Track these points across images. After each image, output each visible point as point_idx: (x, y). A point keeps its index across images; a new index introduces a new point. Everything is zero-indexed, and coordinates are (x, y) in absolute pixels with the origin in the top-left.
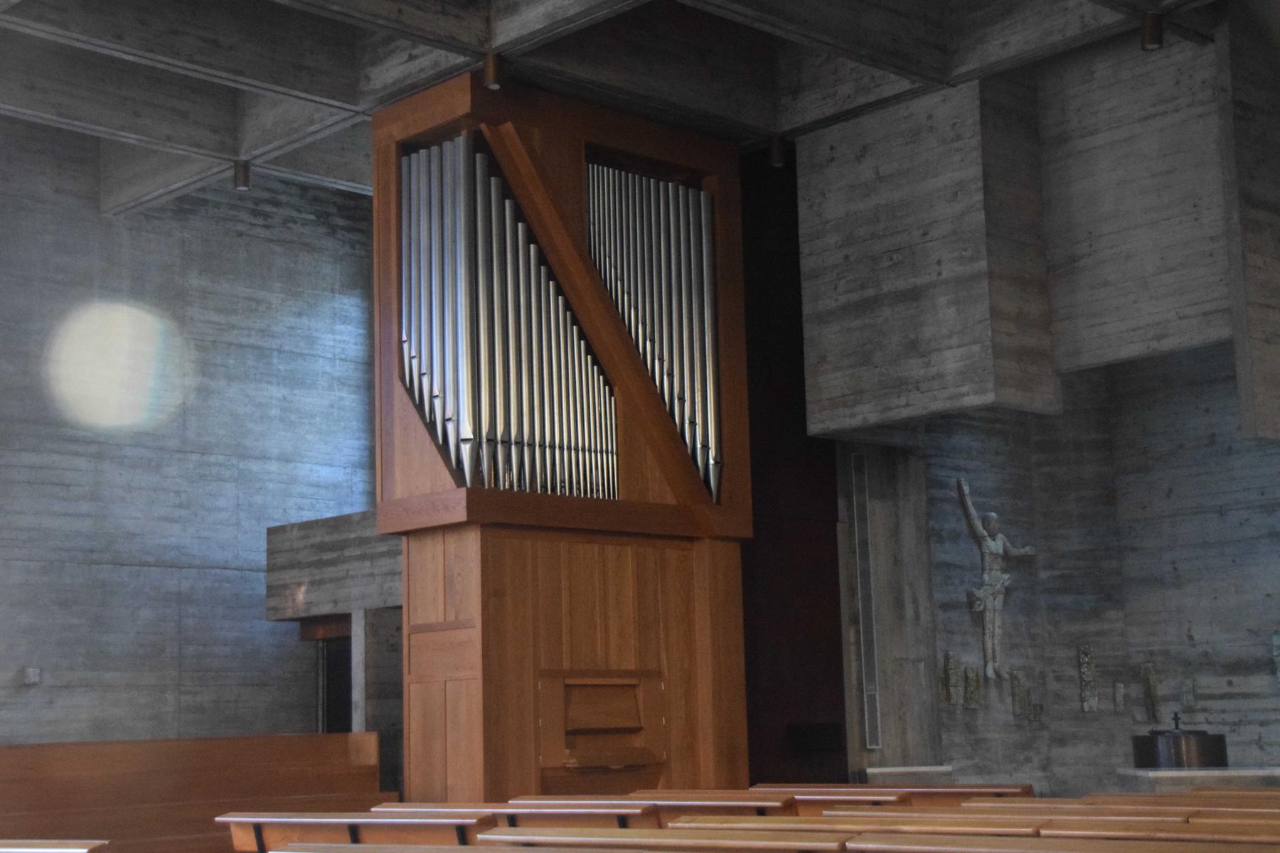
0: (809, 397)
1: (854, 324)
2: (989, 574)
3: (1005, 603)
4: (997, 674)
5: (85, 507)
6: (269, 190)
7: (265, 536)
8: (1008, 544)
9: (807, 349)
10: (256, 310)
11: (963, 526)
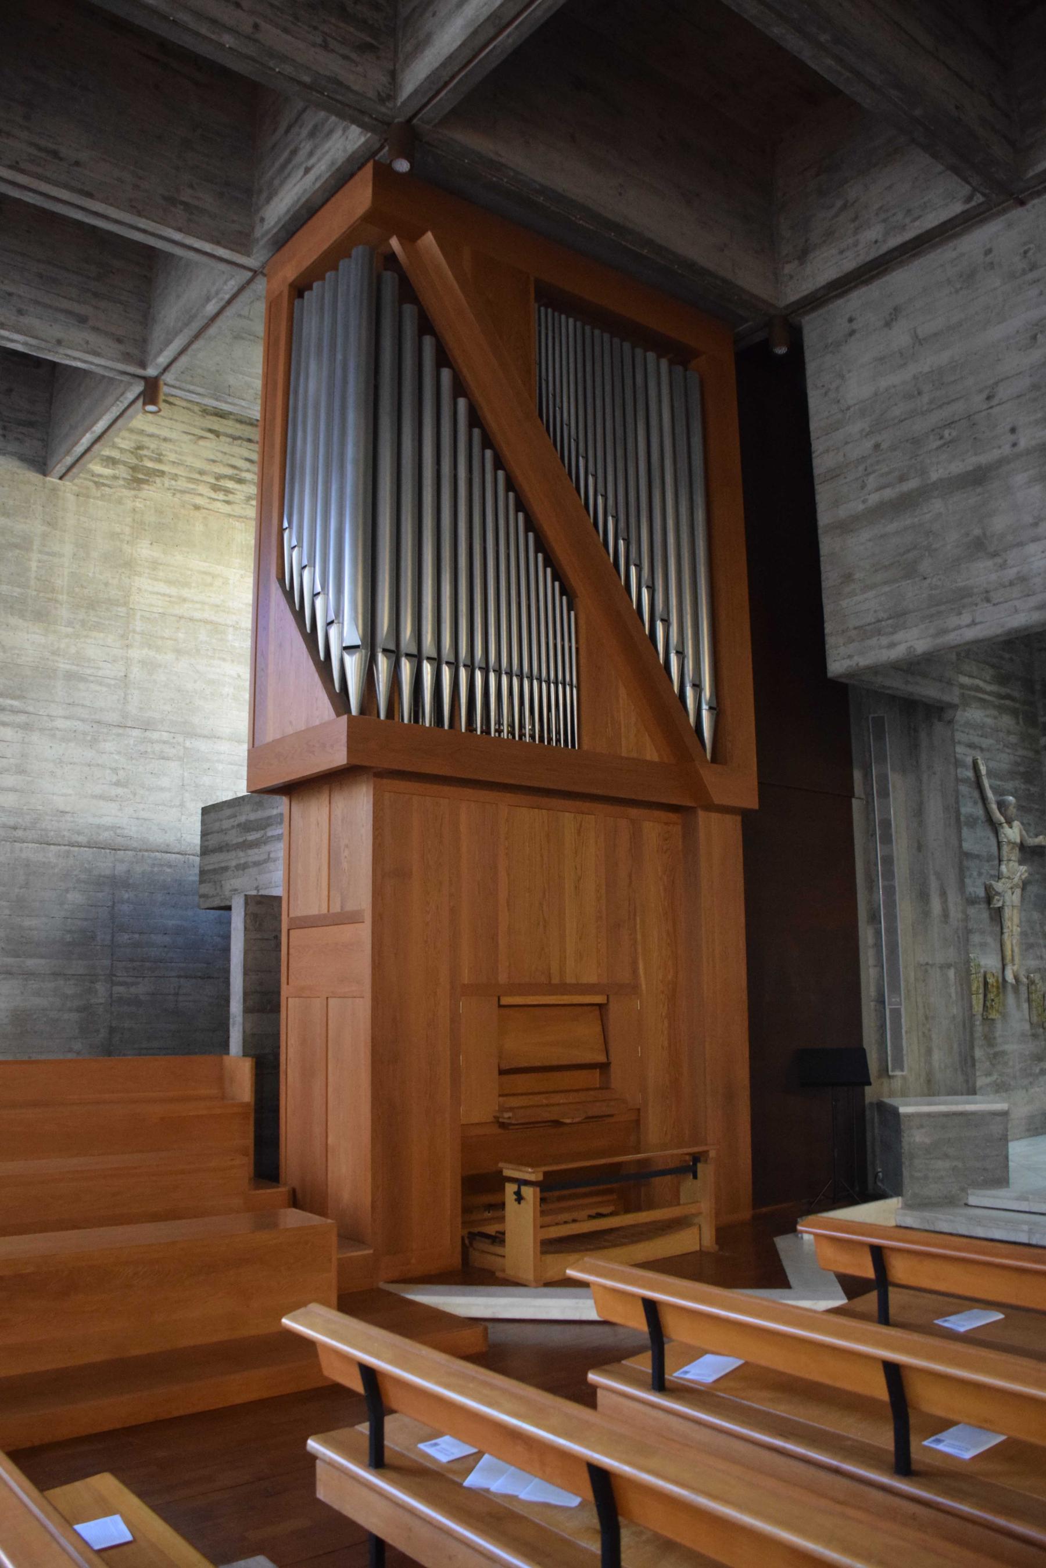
0: (828, 628)
1: (892, 527)
2: (1007, 865)
3: (1023, 898)
4: (1016, 978)
6: (234, 467)
7: (199, 817)
8: (1024, 833)
9: (825, 567)
10: (211, 585)
11: (980, 812)
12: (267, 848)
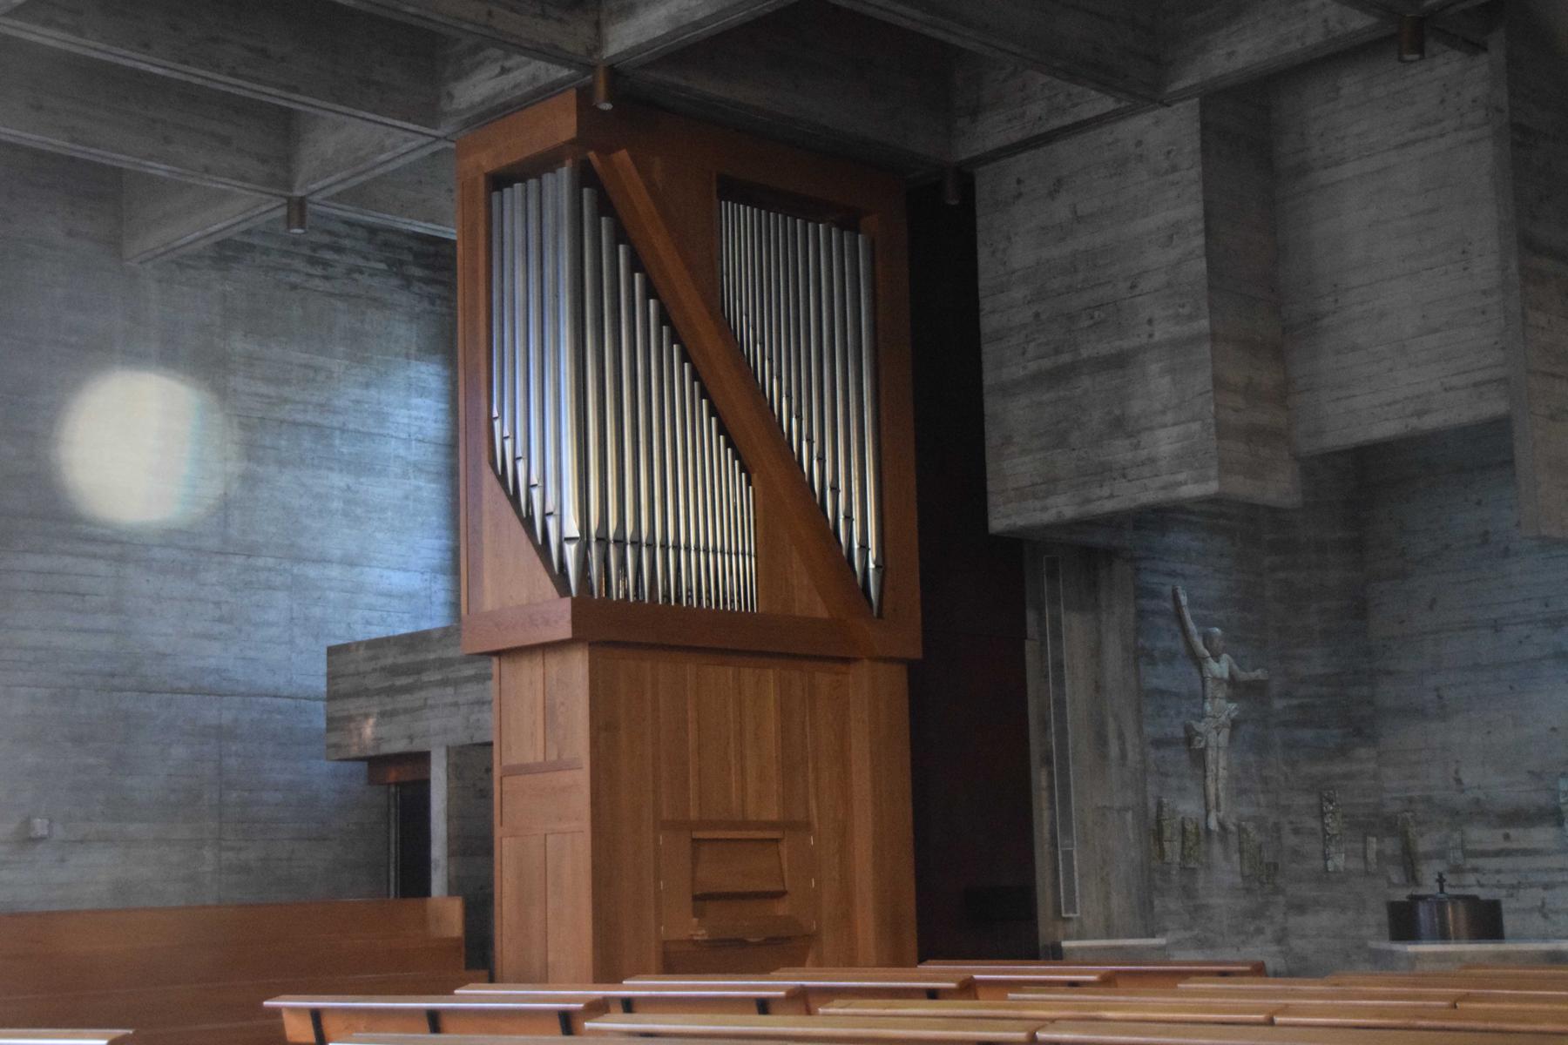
0: (990, 487)
1: (1047, 397)
2: (1212, 704)
3: (1232, 739)
4: (1222, 825)
5: (104, 621)
6: (330, 233)
7: (325, 656)
8: (1235, 667)
9: (988, 427)
10: (314, 380)
11: (1179, 645)
12: (423, 694)
